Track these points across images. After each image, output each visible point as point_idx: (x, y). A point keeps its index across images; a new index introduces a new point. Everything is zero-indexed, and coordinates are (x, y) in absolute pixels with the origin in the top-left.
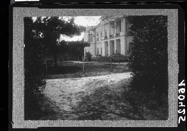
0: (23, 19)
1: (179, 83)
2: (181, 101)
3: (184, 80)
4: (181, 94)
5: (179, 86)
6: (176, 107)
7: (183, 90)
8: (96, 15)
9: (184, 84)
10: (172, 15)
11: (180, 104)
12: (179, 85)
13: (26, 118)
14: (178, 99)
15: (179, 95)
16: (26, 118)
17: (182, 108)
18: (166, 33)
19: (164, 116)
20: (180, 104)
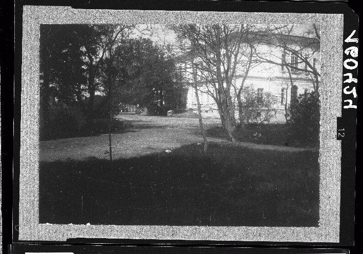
0: (38, 28)
1: (345, 36)
2: (349, 71)
3: (354, 31)
4: (350, 57)
5: (344, 43)
6: (340, 83)
7: (354, 51)
8: (21, 12)
9: (356, 40)
10: (31, 227)
11: (348, 77)
12: (346, 41)
13: (43, 220)
14: (344, 68)
15: (345, 59)
16: (43, 220)
17: (352, 85)
18: (316, 168)
19: (312, 220)
20: (348, 77)
